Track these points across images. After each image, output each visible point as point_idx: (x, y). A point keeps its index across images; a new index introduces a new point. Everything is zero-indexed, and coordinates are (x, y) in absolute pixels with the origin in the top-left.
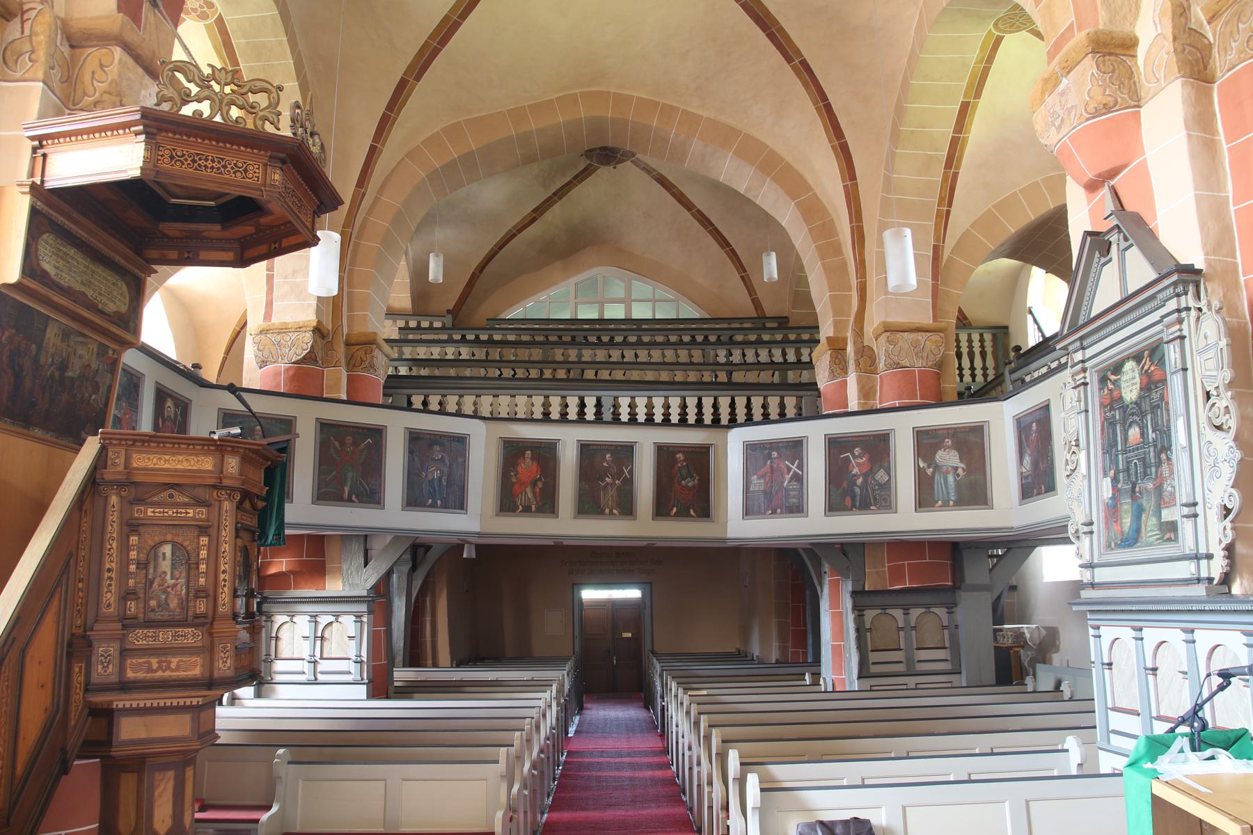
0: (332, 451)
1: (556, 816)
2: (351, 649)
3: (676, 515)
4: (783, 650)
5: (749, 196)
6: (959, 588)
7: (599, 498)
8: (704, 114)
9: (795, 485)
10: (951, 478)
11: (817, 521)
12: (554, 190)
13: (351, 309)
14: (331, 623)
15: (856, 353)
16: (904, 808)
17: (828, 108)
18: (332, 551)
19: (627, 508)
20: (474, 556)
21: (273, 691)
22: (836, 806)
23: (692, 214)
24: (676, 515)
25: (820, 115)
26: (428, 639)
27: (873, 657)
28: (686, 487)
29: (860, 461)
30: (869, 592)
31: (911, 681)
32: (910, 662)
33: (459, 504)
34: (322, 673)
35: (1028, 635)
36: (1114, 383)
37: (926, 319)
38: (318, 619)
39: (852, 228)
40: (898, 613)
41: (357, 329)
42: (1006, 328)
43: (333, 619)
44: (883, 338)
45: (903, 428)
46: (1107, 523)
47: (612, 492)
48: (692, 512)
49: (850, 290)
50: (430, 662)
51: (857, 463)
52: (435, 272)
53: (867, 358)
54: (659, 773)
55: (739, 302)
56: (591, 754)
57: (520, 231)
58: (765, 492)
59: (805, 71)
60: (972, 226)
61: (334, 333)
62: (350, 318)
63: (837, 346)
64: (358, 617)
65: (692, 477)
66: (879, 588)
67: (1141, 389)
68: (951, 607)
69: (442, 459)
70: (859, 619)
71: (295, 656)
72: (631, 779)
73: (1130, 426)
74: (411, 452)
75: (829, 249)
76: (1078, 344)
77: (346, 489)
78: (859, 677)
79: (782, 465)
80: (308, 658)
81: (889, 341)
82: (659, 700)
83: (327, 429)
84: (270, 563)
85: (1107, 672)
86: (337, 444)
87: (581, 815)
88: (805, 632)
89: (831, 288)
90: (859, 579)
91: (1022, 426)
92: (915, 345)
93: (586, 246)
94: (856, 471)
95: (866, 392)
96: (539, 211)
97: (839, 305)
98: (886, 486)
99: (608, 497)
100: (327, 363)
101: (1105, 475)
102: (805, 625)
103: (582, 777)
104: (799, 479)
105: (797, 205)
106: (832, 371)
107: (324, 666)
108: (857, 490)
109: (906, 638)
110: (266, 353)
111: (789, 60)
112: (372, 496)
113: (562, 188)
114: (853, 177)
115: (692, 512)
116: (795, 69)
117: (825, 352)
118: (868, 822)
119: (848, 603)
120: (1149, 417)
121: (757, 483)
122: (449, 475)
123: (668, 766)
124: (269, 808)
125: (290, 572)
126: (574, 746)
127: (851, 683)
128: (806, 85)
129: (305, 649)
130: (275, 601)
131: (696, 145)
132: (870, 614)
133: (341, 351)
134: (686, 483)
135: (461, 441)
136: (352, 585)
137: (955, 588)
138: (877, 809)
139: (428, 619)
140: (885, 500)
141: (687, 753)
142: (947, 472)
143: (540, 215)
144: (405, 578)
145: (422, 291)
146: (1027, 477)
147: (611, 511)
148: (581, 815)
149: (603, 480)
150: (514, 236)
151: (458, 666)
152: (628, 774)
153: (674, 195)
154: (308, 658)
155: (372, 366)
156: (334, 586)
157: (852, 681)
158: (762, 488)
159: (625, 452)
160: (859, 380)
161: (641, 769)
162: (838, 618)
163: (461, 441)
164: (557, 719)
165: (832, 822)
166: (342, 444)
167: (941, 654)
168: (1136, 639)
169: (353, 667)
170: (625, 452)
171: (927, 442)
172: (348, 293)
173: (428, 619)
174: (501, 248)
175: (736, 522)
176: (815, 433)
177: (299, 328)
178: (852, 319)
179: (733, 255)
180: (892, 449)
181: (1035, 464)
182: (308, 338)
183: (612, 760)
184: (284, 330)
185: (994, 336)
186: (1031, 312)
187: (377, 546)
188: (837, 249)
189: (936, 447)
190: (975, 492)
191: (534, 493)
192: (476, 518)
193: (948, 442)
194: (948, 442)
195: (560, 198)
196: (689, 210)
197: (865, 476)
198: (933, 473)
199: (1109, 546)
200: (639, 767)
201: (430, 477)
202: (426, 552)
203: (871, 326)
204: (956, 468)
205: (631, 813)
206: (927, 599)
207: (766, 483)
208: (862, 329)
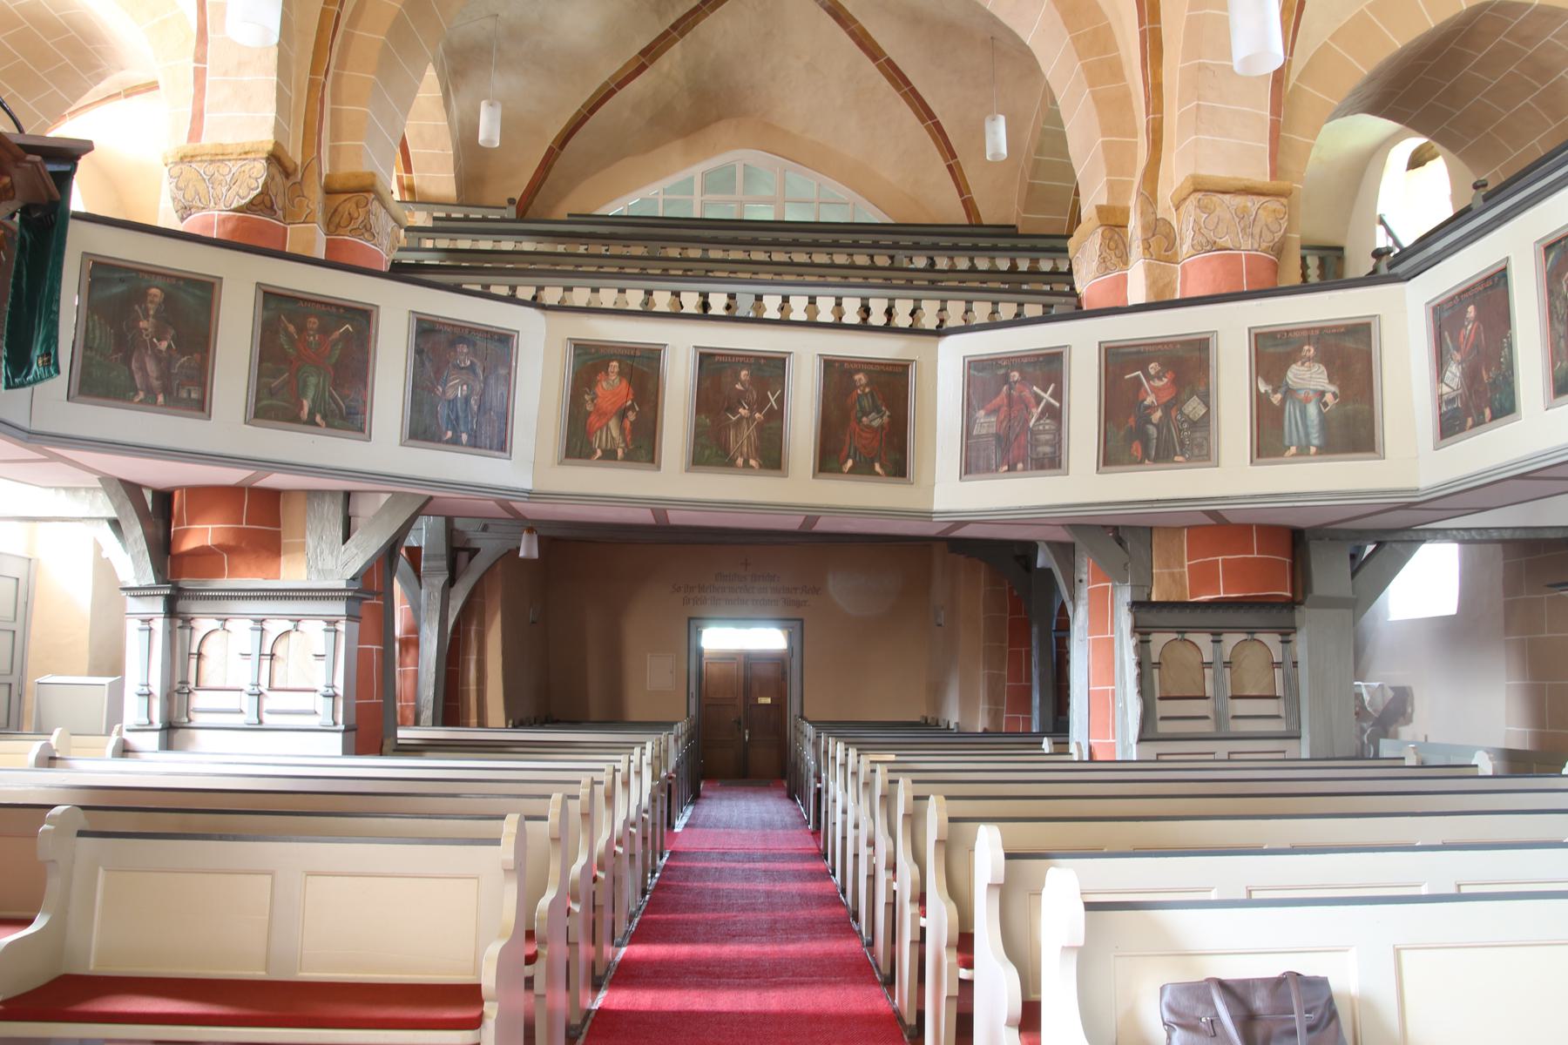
0: (283, 339)
1: (640, 950)
2: (318, 675)
3: (851, 471)
4: (995, 715)
6: (1301, 603)
7: (727, 441)
9: (1048, 424)
10: (1312, 410)
11: (1083, 483)
12: (673, 21)
13: (336, 136)
14: (288, 632)
15: (1145, 228)
16: (1397, 951)
18: (290, 514)
19: (772, 458)
20: (535, 555)
21: (191, 739)
22: (1251, 947)
24: (851, 471)
26: (473, 687)
27: (1163, 708)
28: (869, 427)
29: (1158, 383)
31: (1221, 749)
32: (1219, 717)
33: (501, 445)
34: (271, 712)
35: (1366, 697)
37: (1260, 174)
38: (266, 625)
39: (1143, 34)
40: (1203, 640)
41: (347, 167)
42: (1341, 249)
43: (290, 625)
45: (1231, 330)
47: (748, 432)
48: (877, 468)
49: (1134, 134)
50: (474, 720)
51: (1154, 388)
52: (489, 130)
53: (1161, 240)
54: (813, 887)
55: (946, 207)
56: (707, 855)
57: (621, 85)
58: (998, 437)
60: (1332, 38)
61: (306, 168)
62: (335, 151)
63: (1113, 222)
64: (332, 623)
65: (879, 412)
66: (1174, 598)
68: (1287, 633)
69: (472, 368)
70: (1142, 646)
71: (228, 686)
72: (768, 894)
74: (419, 351)
77: (306, 404)
78: (1141, 740)
79: (1027, 393)
80: (249, 689)
81: (1201, 207)
82: (812, 781)
83: (273, 300)
84: (186, 532)
86: (291, 328)
87: (683, 950)
88: (1029, 690)
90: (1143, 581)
91: (1445, 316)
93: (719, 118)
94: (1150, 399)
96: (651, 53)
97: (1116, 159)
98: (1204, 425)
99: (743, 439)
100: (290, 216)
102: (1029, 678)
103: (690, 890)
104: (1055, 414)
106: (1103, 260)
107: (272, 701)
108: (1152, 431)
109: (1215, 680)
110: (190, 193)
112: (349, 417)
113: (679, 21)
115: (877, 468)
117: (1093, 232)
118: (1321, 983)
119: (1124, 620)
121: (986, 423)
122: (482, 395)
123: (828, 875)
124: (27, 922)
125: (219, 546)
126: (680, 845)
127: (1125, 750)
129: (243, 673)
130: (197, 596)
132: (1159, 640)
133: (315, 198)
134: (871, 419)
135: (504, 339)
136: (322, 573)
137: (1291, 604)
138: (1340, 951)
139: (473, 658)
141: (864, 852)
142: (1307, 400)
143: (652, 61)
144: (438, 595)
145: (473, 165)
146: (1451, 401)
147: (746, 462)
148: (683, 950)
149: (735, 412)
150: (611, 93)
151: (514, 727)
152: (762, 886)
153: (852, 35)
154: (249, 689)
155: (367, 228)
156: (293, 572)
157: (1125, 742)
158: (993, 430)
159: (772, 368)
160: (1149, 271)
161: (784, 880)
162: (1105, 651)
163: (504, 339)
164: (653, 799)
165: (1246, 983)
166: (302, 329)
169: (323, 706)
170: (772, 368)
171: (1273, 353)
172: (332, 110)
173: (473, 658)
174: (592, 111)
175: (950, 487)
176: (1082, 343)
177: (245, 154)
178: (1137, 180)
179: (938, 132)
180: (1212, 362)
181: (1471, 377)
182: (258, 172)
183: (739, 865)
184: (219, 156)
185: (1322, 265)
186: (1382, 222)
187: (364, 510)
188: (1115, 71)
190: (1354, 431)
191: (622, 430)
192: (527, 465)
193: (1309, 350)
194: (1309, 350)
195: (682, 35)
196: (874, 59)
198: (1283, 401)
200: (780, 876)
201: (450, 395)
202: (470, 559)
204: (1322, 394)
205: (768, 949)
208: (1154, 192)
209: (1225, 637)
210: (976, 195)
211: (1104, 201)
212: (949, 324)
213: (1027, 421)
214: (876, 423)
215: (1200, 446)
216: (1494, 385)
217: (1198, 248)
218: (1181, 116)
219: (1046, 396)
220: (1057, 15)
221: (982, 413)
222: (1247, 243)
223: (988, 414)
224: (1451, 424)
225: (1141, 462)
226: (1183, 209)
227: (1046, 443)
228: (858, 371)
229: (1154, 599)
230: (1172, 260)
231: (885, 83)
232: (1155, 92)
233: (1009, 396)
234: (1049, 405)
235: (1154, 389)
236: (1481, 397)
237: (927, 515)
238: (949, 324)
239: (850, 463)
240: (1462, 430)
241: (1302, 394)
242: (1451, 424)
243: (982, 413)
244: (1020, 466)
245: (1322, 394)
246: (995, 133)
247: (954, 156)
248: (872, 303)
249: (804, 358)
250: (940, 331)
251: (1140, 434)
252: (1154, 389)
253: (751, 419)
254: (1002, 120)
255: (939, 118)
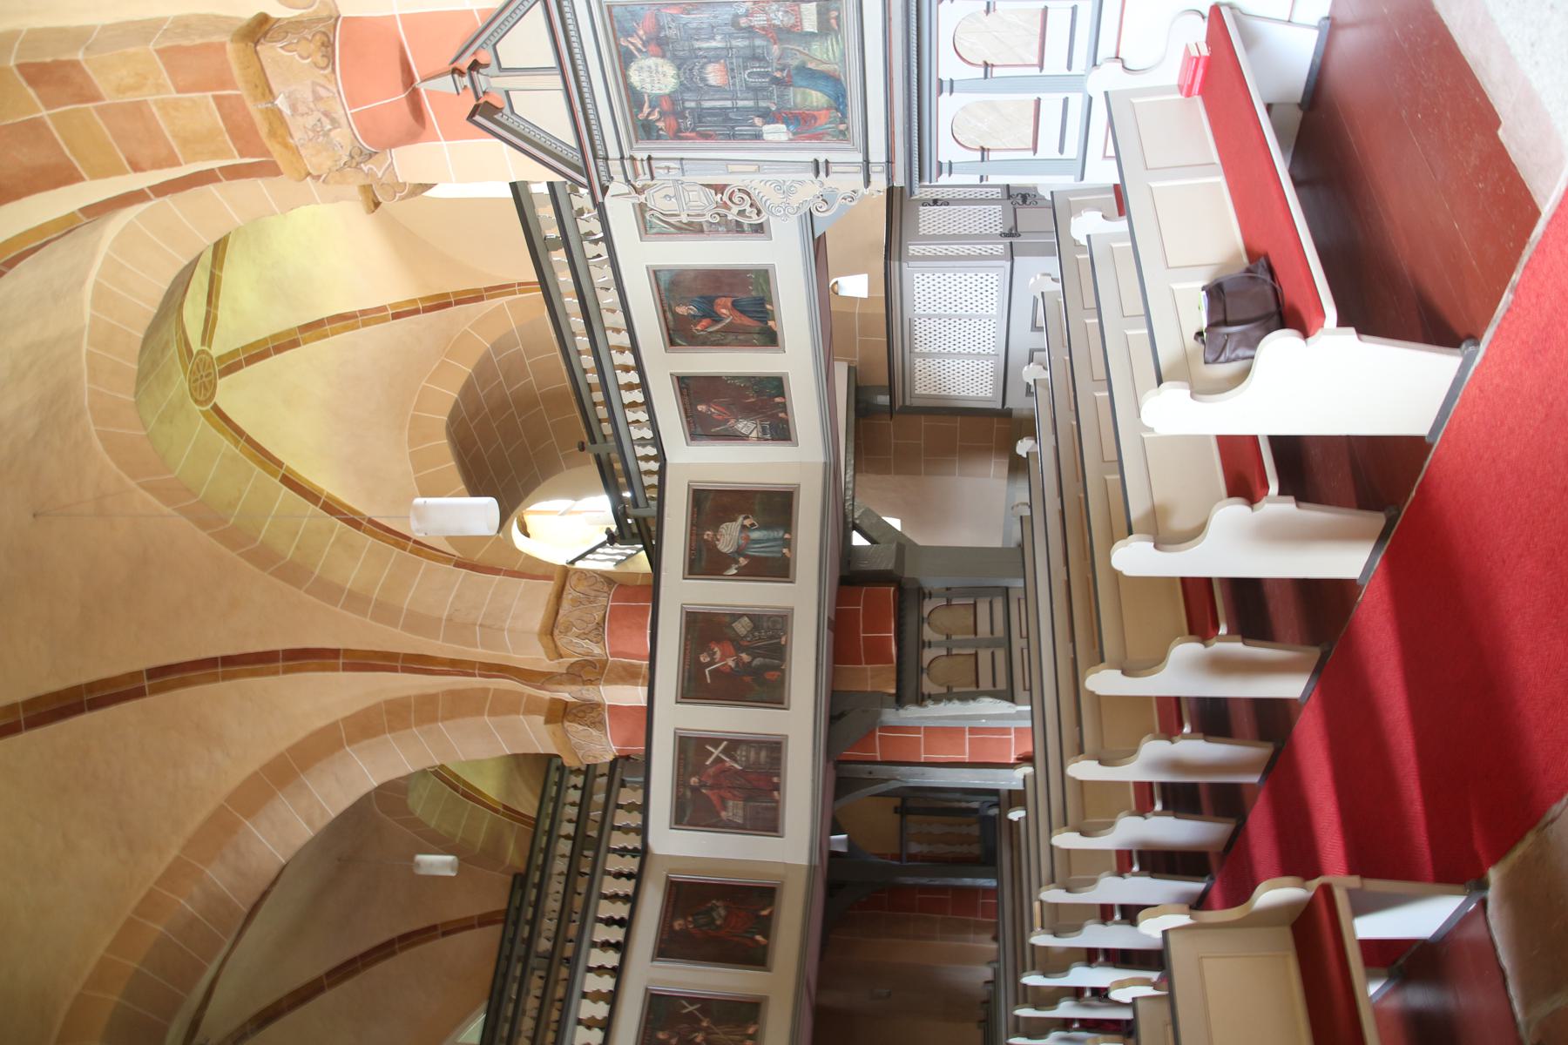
3: (767, 936)
4: (980, 928)
5: (321, 824)
8: (175, 852)
9: (741, 753)
10: (755, 535)
15: (573, 682)
17: (228, 661)
23: (331, 985)
24: (767, 936)
25: (234, 676)
27: (986, 684)
28: (725, 919)
29: (718, 655)
30: (898, 688)
31: (1018, 643)
32: (992, 643)
36: (652, 107)
40: (928, 655)
44: (562, 641)
45: (682, 593)
46: (818, 137)
48: (765, 913)
51: (721, 658)
55: (475, 950)
58: (746, 800)
59: (166, 676)
63: (559, 713)
65: (712, 909)
66: (893, 676)
67: (663, 57)
68: (922, 594)
70: (937, 699)
73: (703, 80)
75: (425, 710)
76: (600, 163)
78: (1012, 700)
79: (711, 771)
85: (996, 72)
89: (480, 712)
90: (880, 699)
91: (699, 429)
92: (576, 602)
95: (628, 676)
97: (505, 706)
98: (756, 619)
101: (758, 136)
104: (734, 745)
105: (351, 742)
106: (593, 724)
108: (758, 661)
111: (139, 693)
114: (335, 653)
115: (765, 913)
116: (156, 690)
120: (697, 45)
121: (734, 810)
128: (185, 683)
131: (218, 876)
132: (928, 686)
134: (717, 918)
137: (901, 590)
140: (775, 622)
142: (747, 538)
146: (764, 431)
160: (610, 681)
167: (983, 608)
168: (951, 92)
171: (704, 562)
175: (788, 849)
181: (749, 411)
186: (573, 562)
189: (712, 547)
193: (708, 535)
194: (708, 535)
197: (739, 648)
198: (746, 556)
199: (843, 133)
203: (546, 664)
204: (744, 527)
206: (911, 620)
207: (735, 797)
209: (926, 638)
210: (475, 911)
211: (541, 719)
212: (638, 845)
213: (737, 771)
214: (723, 912)
215: (775, 622)
216: (759, 393)
217: (599, 640)
218: (483, 646)
219: (716, 753)
220: (366, 743)
221: (723, 814)
222: (602, 600)
223: (725, 808)
224: (780, 431)
225: (783, 671)
226: (563, 650)
227: (758, 754)
228: (671, 926)
229: (893, 691)
230: (604, 663)
231: (347, 985)
232: (458, 667)
233: (712, 787)
234: (724, 751)
235: (722, 659)
236: (764, 405)
237: (812, 868)
238: (638, 845)
239: (759, 938)
240: (787, 422)
241: (742, 542)
242: (780, 431)
243: (723, 814)
244: (775, 780)
245: (744, 527)
246: (431, 865)
247: (434, 928)
248: (598, 938)
249: (650, 973)
250: (643, 853)
251: (757, 673)
252: (722, 659)
253: (707, 1030)
254: (420, 858)
255: (394, 935)
